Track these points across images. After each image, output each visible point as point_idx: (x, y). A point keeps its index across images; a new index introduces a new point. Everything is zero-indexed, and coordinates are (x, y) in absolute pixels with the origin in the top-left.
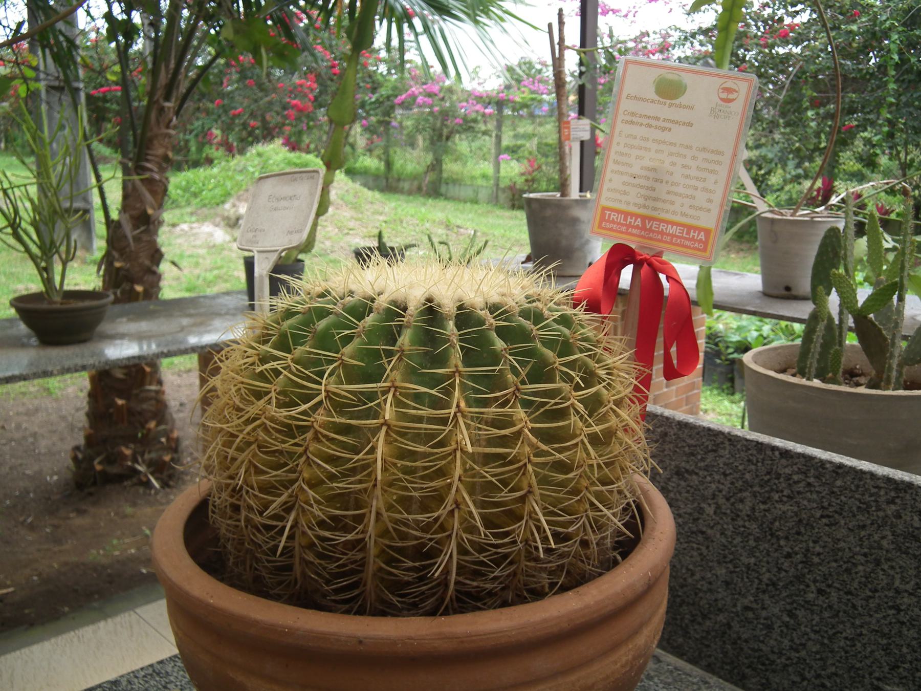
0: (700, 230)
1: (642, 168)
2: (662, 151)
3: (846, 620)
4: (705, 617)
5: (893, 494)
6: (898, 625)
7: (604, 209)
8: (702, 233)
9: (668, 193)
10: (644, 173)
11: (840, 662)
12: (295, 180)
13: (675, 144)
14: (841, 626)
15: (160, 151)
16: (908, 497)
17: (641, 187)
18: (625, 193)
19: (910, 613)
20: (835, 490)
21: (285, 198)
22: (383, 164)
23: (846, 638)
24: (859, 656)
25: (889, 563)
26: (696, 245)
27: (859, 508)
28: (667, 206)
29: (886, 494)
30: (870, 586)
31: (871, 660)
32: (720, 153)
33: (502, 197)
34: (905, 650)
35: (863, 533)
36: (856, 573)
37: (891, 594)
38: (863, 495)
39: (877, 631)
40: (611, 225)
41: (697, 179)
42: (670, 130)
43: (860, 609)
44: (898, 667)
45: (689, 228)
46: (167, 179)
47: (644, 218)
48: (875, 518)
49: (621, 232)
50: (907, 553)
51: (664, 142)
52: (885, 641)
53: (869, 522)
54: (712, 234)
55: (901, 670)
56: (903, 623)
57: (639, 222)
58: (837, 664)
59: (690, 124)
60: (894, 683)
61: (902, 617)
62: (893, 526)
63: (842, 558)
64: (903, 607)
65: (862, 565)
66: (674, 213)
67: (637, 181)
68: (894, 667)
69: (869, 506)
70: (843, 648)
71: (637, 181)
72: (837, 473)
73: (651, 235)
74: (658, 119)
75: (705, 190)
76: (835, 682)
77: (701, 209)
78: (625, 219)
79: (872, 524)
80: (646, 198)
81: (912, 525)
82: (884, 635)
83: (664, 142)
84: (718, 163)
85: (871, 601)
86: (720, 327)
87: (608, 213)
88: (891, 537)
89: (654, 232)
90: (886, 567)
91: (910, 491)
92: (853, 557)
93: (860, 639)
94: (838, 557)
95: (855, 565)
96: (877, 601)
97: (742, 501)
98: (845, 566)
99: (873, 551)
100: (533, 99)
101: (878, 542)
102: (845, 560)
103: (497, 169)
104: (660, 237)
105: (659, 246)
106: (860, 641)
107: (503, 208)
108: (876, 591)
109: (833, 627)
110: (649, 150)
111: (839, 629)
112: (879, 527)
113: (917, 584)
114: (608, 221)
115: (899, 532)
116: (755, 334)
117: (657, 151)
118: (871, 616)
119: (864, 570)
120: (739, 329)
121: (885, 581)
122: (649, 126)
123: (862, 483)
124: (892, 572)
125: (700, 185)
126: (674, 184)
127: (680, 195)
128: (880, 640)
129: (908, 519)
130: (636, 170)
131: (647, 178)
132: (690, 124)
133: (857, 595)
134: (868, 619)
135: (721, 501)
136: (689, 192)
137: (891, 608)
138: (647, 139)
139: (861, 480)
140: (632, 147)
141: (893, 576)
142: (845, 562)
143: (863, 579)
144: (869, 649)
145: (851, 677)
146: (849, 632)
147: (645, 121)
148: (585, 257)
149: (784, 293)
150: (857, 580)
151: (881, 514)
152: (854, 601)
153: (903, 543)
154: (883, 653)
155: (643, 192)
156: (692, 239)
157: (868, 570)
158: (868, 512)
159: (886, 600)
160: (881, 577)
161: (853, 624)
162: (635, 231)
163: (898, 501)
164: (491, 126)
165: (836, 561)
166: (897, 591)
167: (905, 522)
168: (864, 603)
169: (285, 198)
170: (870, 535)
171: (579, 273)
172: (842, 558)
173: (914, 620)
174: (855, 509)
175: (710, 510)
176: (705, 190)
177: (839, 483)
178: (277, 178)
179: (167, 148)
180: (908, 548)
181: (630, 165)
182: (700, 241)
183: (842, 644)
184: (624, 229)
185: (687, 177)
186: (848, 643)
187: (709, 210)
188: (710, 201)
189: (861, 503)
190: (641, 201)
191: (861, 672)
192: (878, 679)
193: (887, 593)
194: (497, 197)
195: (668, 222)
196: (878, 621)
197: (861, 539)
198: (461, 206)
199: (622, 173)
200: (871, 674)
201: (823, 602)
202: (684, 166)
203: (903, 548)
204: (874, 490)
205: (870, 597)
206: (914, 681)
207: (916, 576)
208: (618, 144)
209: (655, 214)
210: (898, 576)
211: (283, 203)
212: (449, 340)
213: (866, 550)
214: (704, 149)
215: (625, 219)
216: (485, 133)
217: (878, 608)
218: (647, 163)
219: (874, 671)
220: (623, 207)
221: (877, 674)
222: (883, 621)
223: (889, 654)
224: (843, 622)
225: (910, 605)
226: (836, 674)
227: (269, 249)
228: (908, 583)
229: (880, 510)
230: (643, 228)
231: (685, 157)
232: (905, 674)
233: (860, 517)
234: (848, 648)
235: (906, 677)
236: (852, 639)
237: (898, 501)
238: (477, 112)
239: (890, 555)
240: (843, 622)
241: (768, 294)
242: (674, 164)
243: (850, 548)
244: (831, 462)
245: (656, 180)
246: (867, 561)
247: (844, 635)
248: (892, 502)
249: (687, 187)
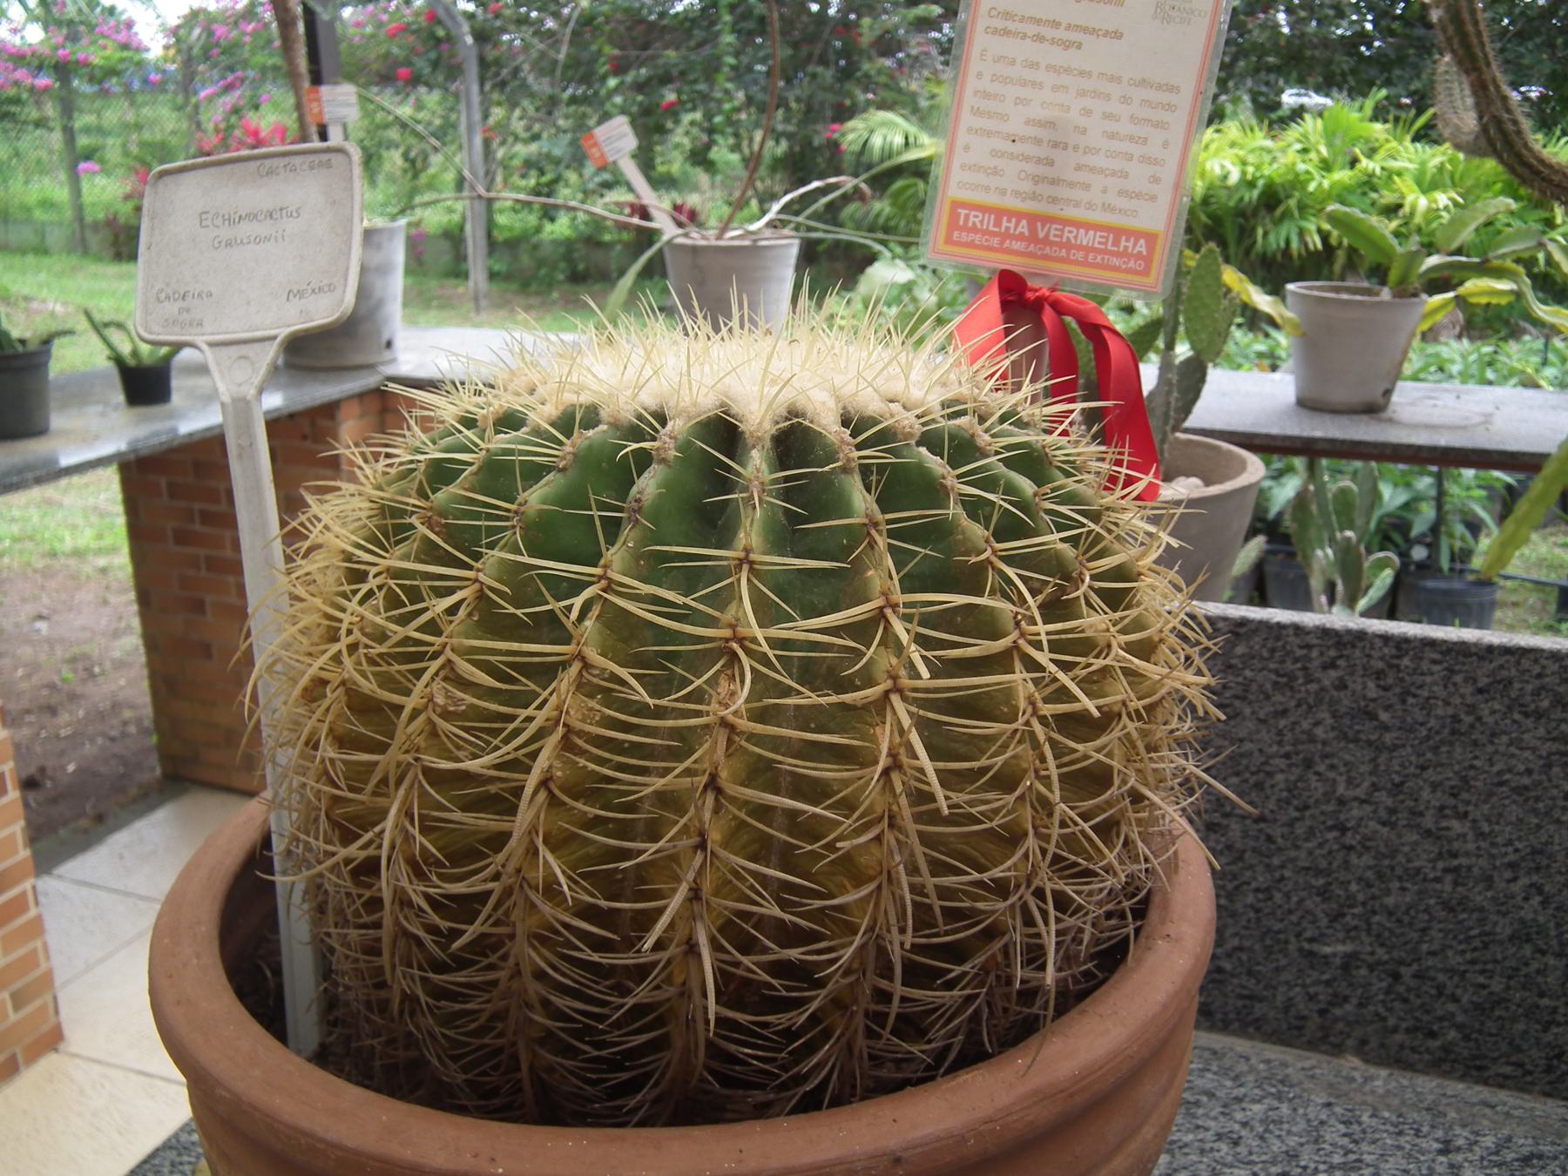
0: (1136, 234)
1: (1028, 122)
2: (1065, 88)
3: (1254, 861)
5: (1333, 653)
6: (1342, 854)
7: (956, 205)
8: (1142, 241)
9: (1079, 168)
10: (1032, 131)
11: (1246, 928)
12: (270, 173)
13: (1090, 74)
14: (1248, 874)
16: (1358, 653)
17: (1027, 158)
18: (996, 172)
19: (1362, 830)
20: (1234, 661)
21: (252, 217)
23: (1257, 890)
24: (1279, 912)
25: (1328, 762)
26: (1131, 264)
27: (1276, 683)
29: (1322, 654)
30: (1295, 802)
31: (1299, 914)
33: (94, 240)
34: (1354, 887)
35: (1282, 723)
36: (1273, 786)
37: (1330, 808)
38: (1282, 662)
39: (1308, 869)
40: (972, 236)
41: (1131, 139)
42: (1079, 46)
43: (1279, 840)
44: (1343, 915)
45: (1118, 233)
47: (1033, 219)
48: (1303, 695)
49: (991, 249)
50: (1356, 741)
51: (1068, 70)
52: (1321, 881)
53: (1293, 703)
54: (1160, 242)
55: (1348, 918)
56: (1350, 848)
57: (1023, 228)
58: (1243, 932)
59: (1117, 35)
60: (1338, 940)
61: (1349, 839)
62: (1333, 702)
63: (1247, 768)
64: (1349, 825)
65: (1282, 771)
66: (1090, 206)
67: (1018, 148)
68: (1337, 917)
69: (1292, 677)
70: (1252, 906)
71: (1018, 148)
72: (1237, 635)
73: (1047, 250)
74: (1056, 24)
75: (1146, 160)
76: (1240, 959)
77: (1138, 196)
78: (998, 224)
79: (1298, 705)
80: (1037, 180)
81: (1364, 698)
82: (1319, 872)
83: (1068, 70)
84: (1169, 107)
85: (1297, 825)
87: (963, 212)
88: (1330, 721)
89: (1052, 244)
90: (1321, 768)
91: (1360, 645)
92: (1266, 763)
93: (1281, 886)
94: (1241, 768)
95: (1270, 774)
96: (1308, 823)
98: (1253, 780)
99: (1301, 747)
100: (122, 60)
101: (1309, 733)
102: (1253, 769)
103: (76, 191)
104: (1063, 253)
106: (1280, 890)
107: (99, 259)
108: (1306, 807)
109: (1235, 877)
110: (1040, 86)
111: (1244, 879)
112: (1310, 707)
113: (1373, 785)
114: (961, 229)
115: (1343, 710)
117: (1055, 89)
118: (1297, 847)
119: (1287, 780)
121: (1321, 790)
122: (1040, 38)
123: (1280, 644)
124: (1331, 775)
125: (1136, 150)
126: (1088, 151)
127: (1102, 171)
128: (1313, 882)
129: (1359, 687)
130: (1016, 126)
132: (1117, 35)
133: (1275, 820)
134: (1293, 853)
136: (1116, 165)
137: (1331, 829)
138: (1034, 65)
139: (1278, 639)
140: (1006, 80)
141: (1334, 781)
142: (1253, 774)
143: (1285, 794)
144: (1295, 899)
145: (1266, 947)
146: (1262, 879)
147: (1032, 29)
148: (378, 332)
150: (1274, 798)
151: (1313, 687)
152: (1269, 831)
153: (1350, 727)
154: (1318, 899)
155: (1031, 168)
156: (1123, 254)
157: (1292, 778)
158: (1292, 688)
159: (1322, 818)
160: (1313, 784)
161: (1268, 866)
162: (1017, 245)
163: (1341, 662)
164: (51, 110)
165: (1237, 774)
166: (1342, 802)
167: (1354, 692)
168: (1286, 830)
169: (252, 217)
170: (1294, 723)
171: (371, 359)
172: (1247, 768)
173: (1369, 840)
174: (1268, 686)
176: (1146, 160)
177: (1240, 650)
178: (212, 170)
180: (1359, 732)
181: (1004, 117)
182: (1139, 256)
183: (1250, 899)
184: (995, 242)
185: (1113, 136)
186: (1261, 896)
187: (1153, 198)
188: (1156, 180)
189: (1278, 675)
190: (1027, 186)
191: (1282, 936)
192: (1311, 940)
193: (1324, 807)
194: (83, 240)
195: (1078, 225)
196: (1310, 853)
197: (1280, 733)
198: (17, 260)
199: (989, 134)
200: (1298, 935)
201: (1218, 842)
202: (1107, 116)
203: (1351, 734)
204: (1300, 652)
205: (1297, 819)
206: (1369, 931)
207: (1371, 773)
208: (979, 75)
210: (1342, 780)
211: (246, 229)
212: (746, 489)
213: (1288, 748)
214: (1143, 83)
215: (998, 224)
216: (39, 124)
217: (1311, 833)
218: (1037, 112)
219: (1305, 929)
220: (992, 200)
221: (1308, 934)
222: (1318, 852)
223: (1329, 899)
224: (1251, 867)
225: (1362, 819)
226: (1241, 949)
227: (259, 334)
228: (1358, 786)
229: (1311, 681)
230: (1032, 238)
231: (1108, 97)
232: (1356, 922)
233: (1278, 698)
234: (1261, 905)
235: (1356, 928)
236: (1268, 889)
237: (1341, 662)
238: (16, 83)
239: (1328, 749)
240: (1251, 867)
242: (1087, 112)
243: (1261, 750)
244: (1225, 619)
245: (1055, 145)
246: (1290, 766)
247: (1254, 885)
248: (1332, 665)
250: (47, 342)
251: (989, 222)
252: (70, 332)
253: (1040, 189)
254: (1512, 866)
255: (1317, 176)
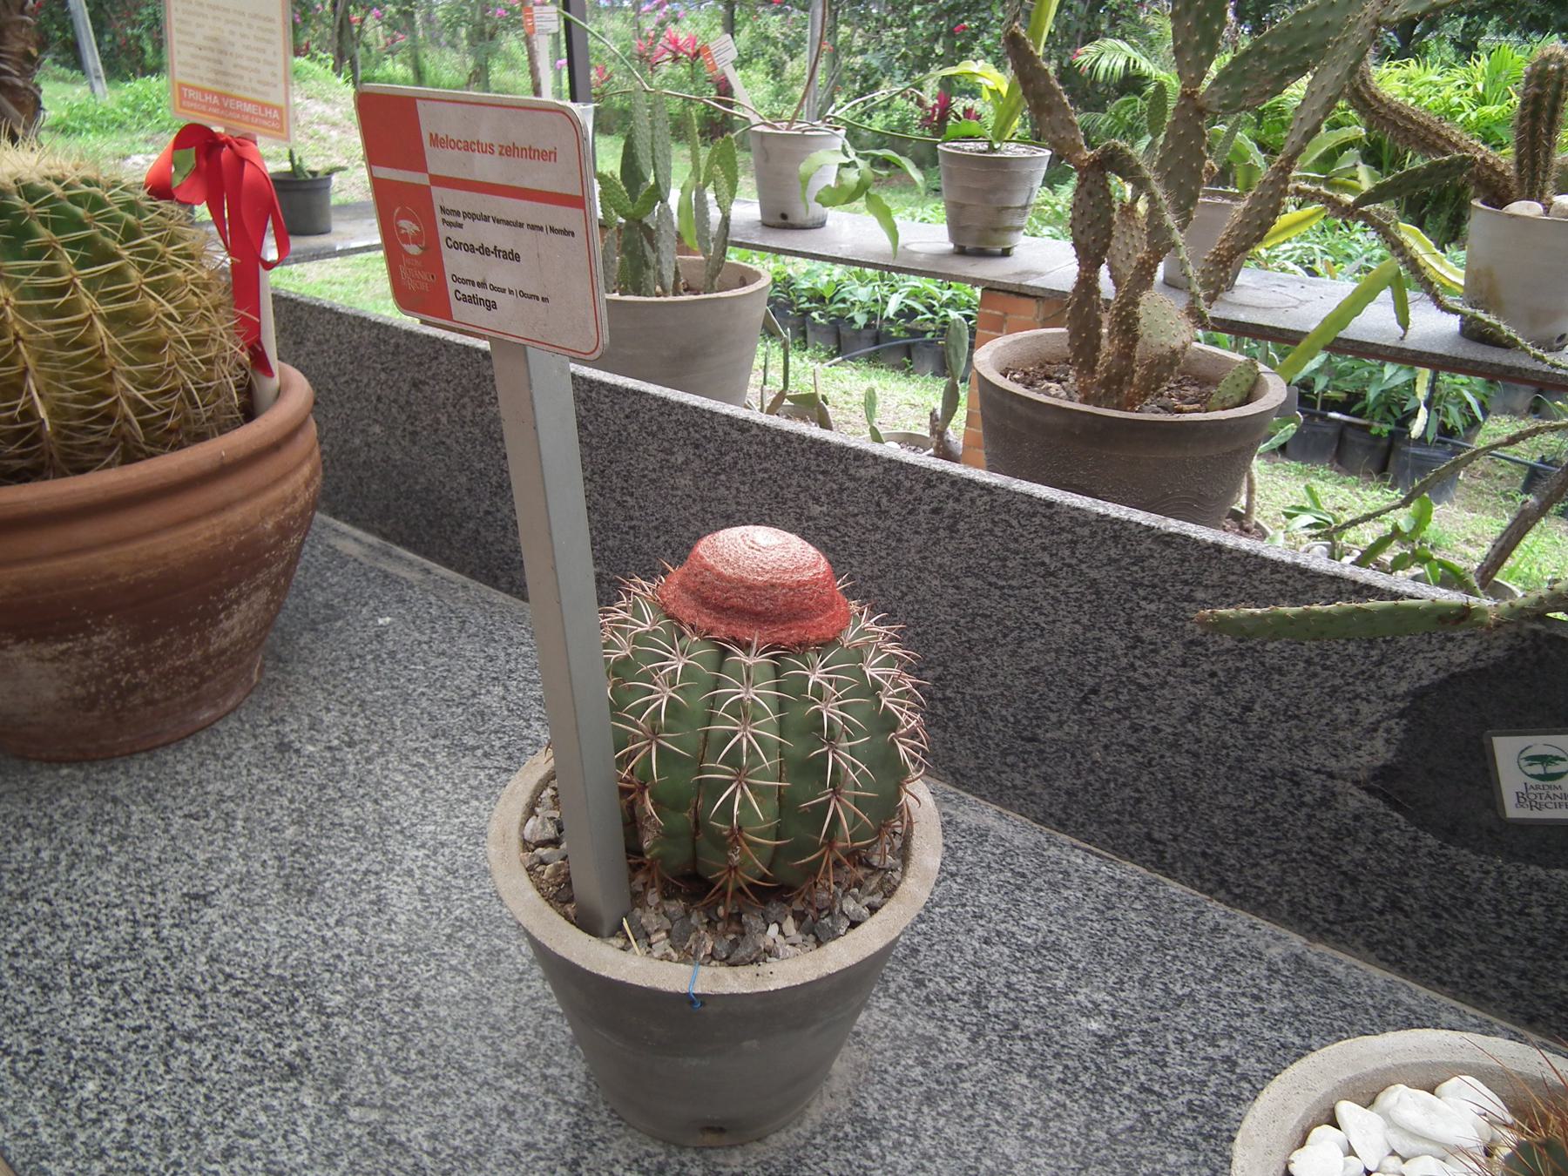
4: (460, 526)
15: (18, 47)
18: (195, 67)
22: (410, 71)
28: (237, 82)
32: (271, 20)
41: (257, 49)
45: (264, 106)
46: (36, 85)
47: (221, 95)
67: (203, 53)
71: (203, 53)
86: (790, 271)
97: (464, 406)
105: (244, 128)
116: (826, 279)
120: (808, 273)
131: (212, 50)
135: (451, 409)
149: (781, 221)
156: (267, 119)
175: (444, 419)
179: (28, 43)
185: (248, 47)
188: (274, 75)
195: (243, 100)
209: (227, 91)
214: (255, 16)
220: (197, 83)
241: (767, 225)
249: (250, 59)
250: (330, 173)
251: (198, 96)
252: (343, 169)
253: (219, 77)
254: (656, 528)
255: (1468, 110)
